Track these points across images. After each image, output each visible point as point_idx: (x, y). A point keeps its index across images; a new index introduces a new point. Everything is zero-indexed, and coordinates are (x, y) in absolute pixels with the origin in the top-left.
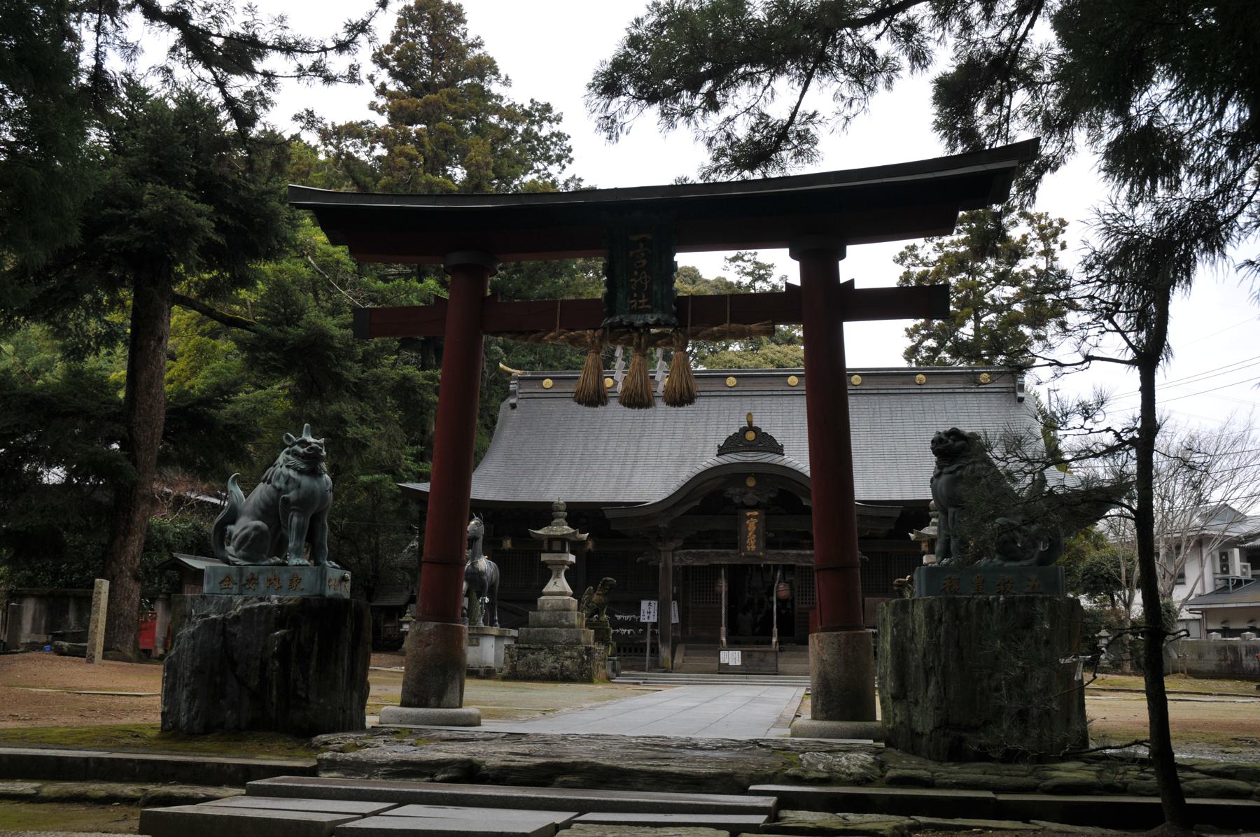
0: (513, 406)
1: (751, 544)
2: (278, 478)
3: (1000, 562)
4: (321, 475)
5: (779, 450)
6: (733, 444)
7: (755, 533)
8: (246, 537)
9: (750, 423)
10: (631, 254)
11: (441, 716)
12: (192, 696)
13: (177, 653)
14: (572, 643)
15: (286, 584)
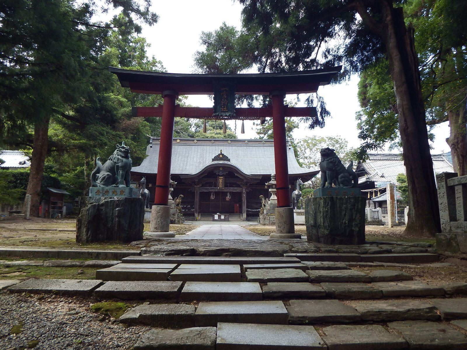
0: (151, 147)
2: (115, 159)
3: (342, 187)
5: (229, 160)
6: (216, 158)
8: (104, 178)
9: (221, 153)
10: (222, 94)
11: (164, 234)
12: (87, 231)
13: (82, 216)
15: (119, 193)
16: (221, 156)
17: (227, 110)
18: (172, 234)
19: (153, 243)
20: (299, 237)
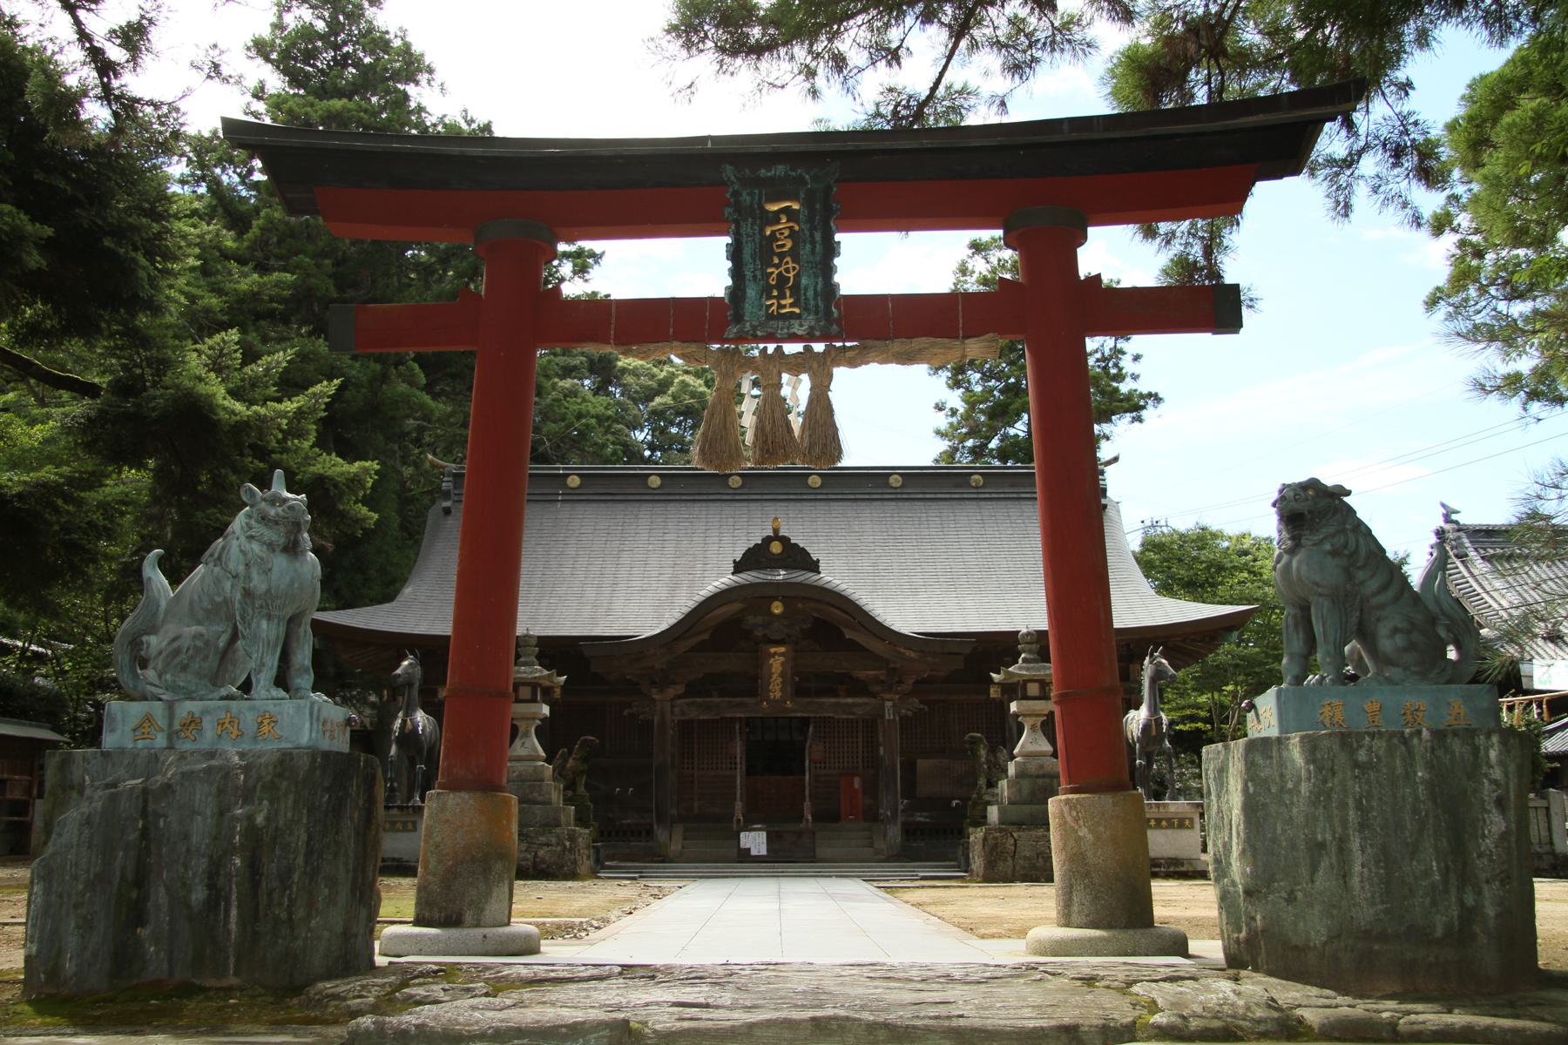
0: (447, 511)
1: (775, 691)
4: (303, 552)
5: (814, 567)
6: (753, 559)
7: (782, 675)
9: (776, 531)
14: (547, 825)
16: (776, 548)
17: (797, 311)
18: (528, 937)
19: (420, 992)
20: (1178, 946)
